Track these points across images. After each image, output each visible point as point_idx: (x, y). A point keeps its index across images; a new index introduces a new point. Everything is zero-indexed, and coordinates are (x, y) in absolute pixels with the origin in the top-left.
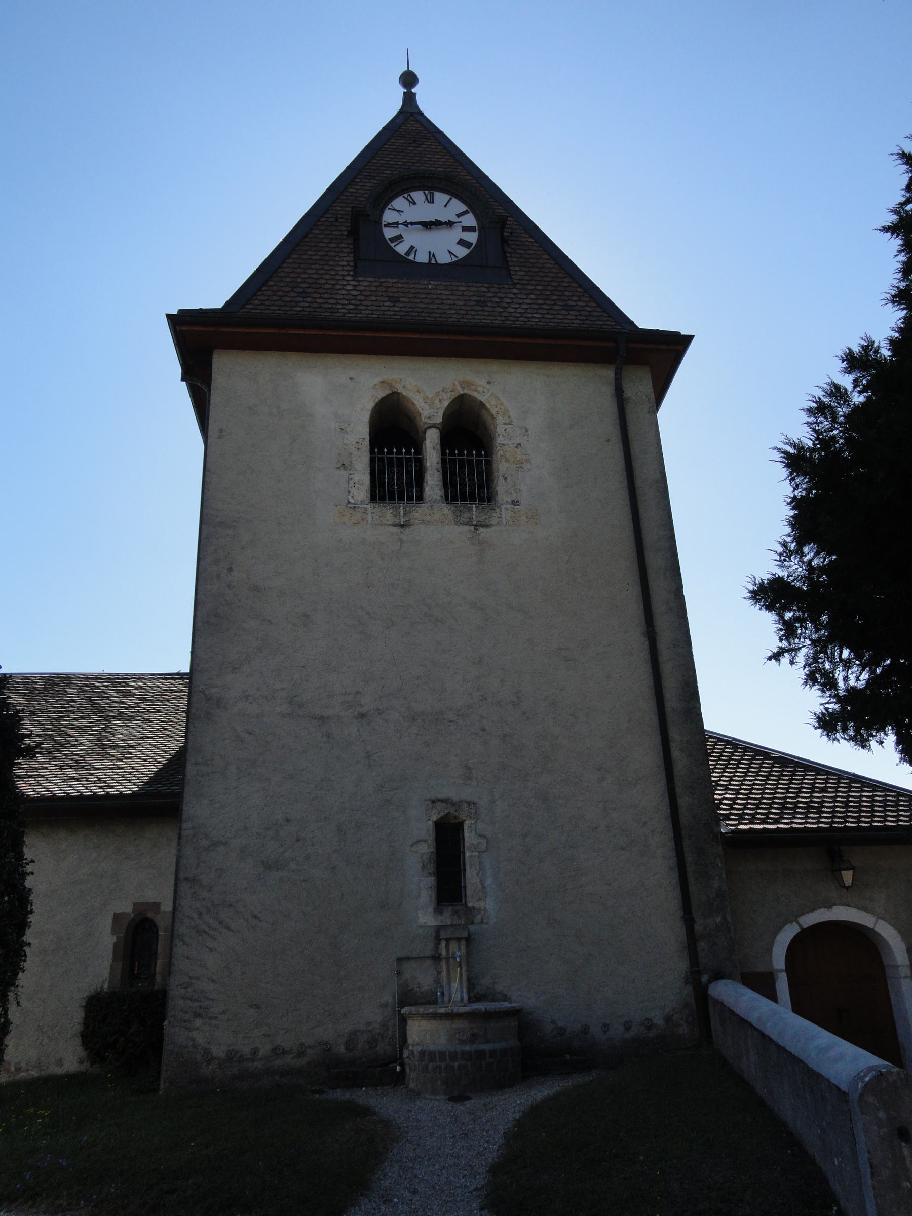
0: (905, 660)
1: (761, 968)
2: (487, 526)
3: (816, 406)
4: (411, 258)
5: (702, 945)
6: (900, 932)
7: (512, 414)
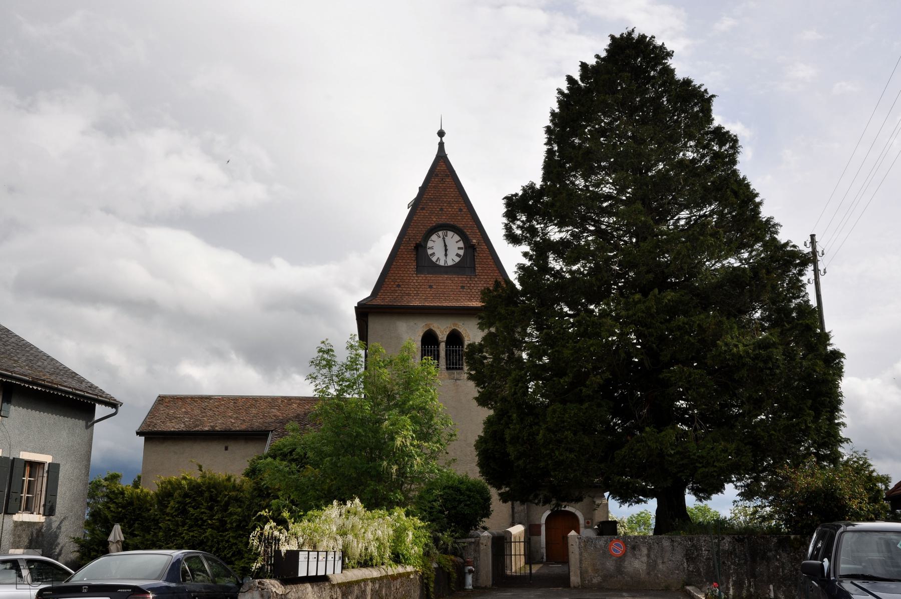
0: (673, 405)
1: (537, 523)
2: (459, 380)
3: (492, 412)
5: (516, 515)
6: (583, 514)
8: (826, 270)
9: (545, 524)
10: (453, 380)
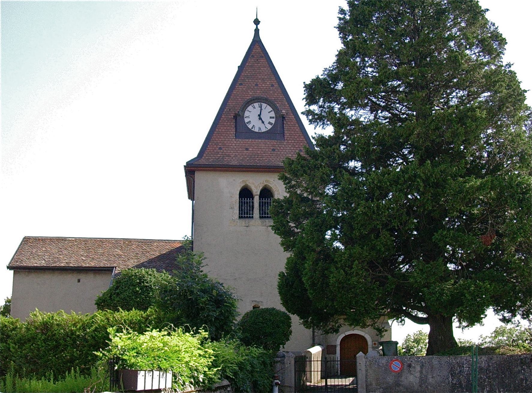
1: (333, 344)
4: (253, 130)
5: (316, 338)
7: (280, 191)
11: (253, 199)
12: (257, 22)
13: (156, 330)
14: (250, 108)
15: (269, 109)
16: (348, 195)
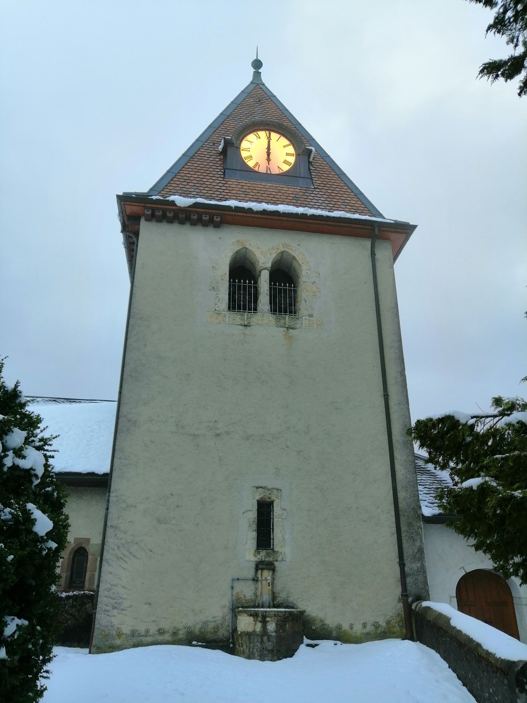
2: (293, 328)
5: (409, 580)
8: (257, 486)
9: (457, 597)
10: (283, 329)
11: (256, 282)
12: (257, 64)
13: (424, 450)
14: (251, 137)
15: (284, 141)
16: (44, 672)
